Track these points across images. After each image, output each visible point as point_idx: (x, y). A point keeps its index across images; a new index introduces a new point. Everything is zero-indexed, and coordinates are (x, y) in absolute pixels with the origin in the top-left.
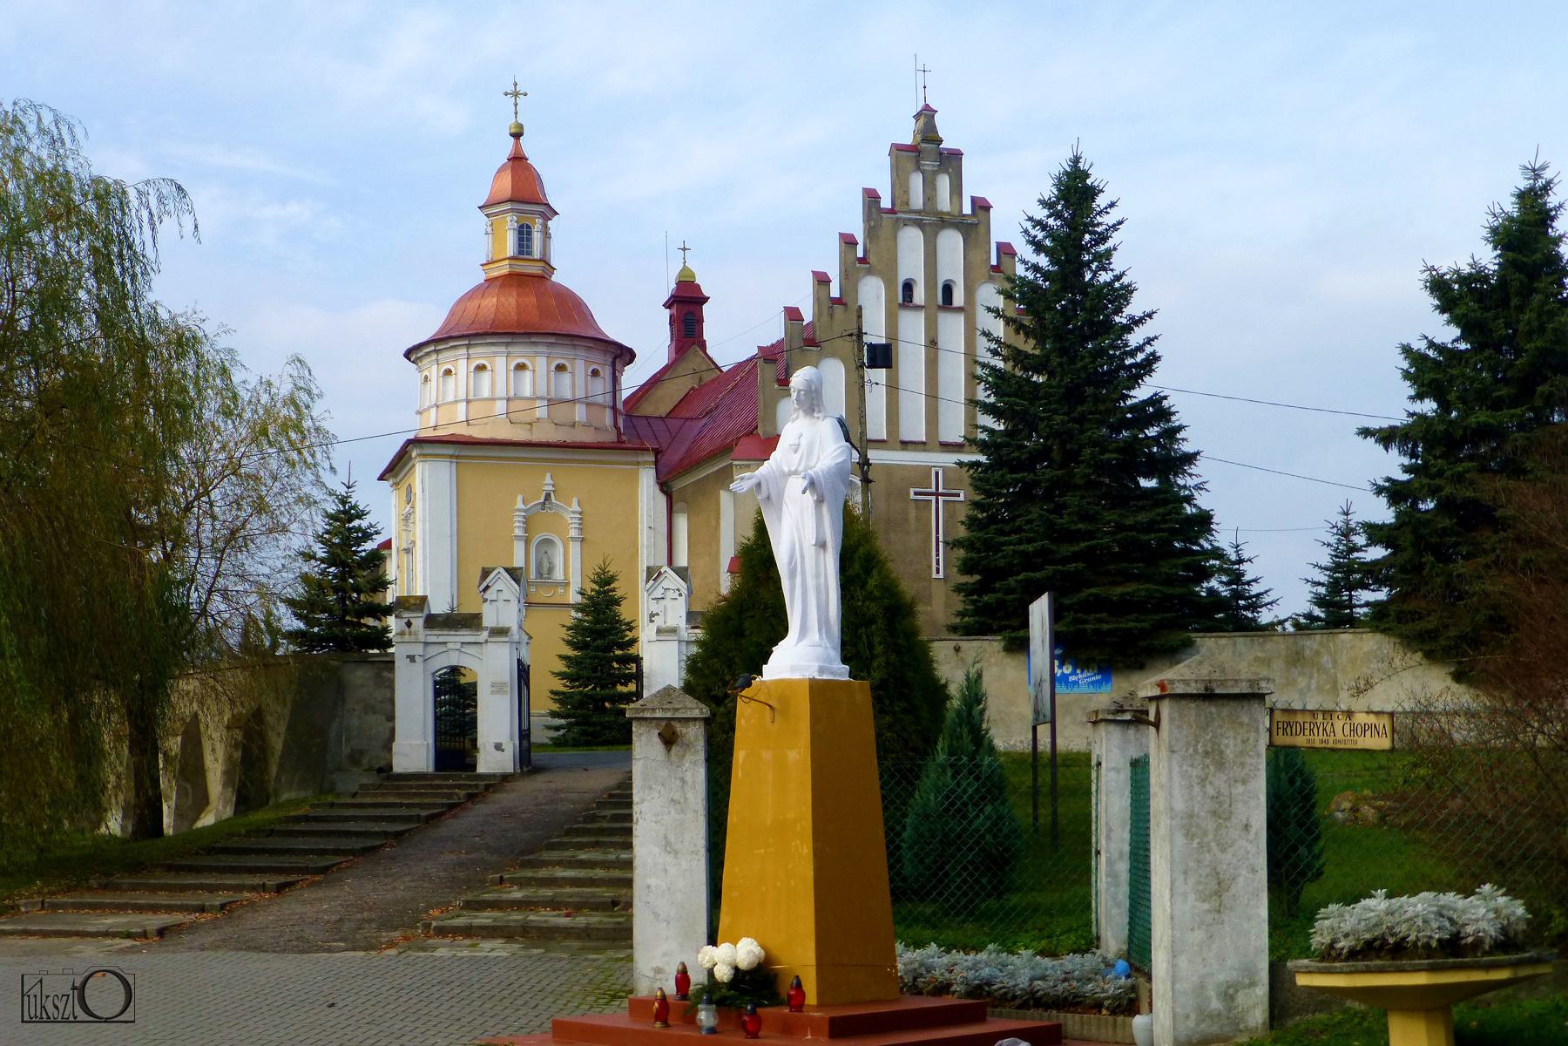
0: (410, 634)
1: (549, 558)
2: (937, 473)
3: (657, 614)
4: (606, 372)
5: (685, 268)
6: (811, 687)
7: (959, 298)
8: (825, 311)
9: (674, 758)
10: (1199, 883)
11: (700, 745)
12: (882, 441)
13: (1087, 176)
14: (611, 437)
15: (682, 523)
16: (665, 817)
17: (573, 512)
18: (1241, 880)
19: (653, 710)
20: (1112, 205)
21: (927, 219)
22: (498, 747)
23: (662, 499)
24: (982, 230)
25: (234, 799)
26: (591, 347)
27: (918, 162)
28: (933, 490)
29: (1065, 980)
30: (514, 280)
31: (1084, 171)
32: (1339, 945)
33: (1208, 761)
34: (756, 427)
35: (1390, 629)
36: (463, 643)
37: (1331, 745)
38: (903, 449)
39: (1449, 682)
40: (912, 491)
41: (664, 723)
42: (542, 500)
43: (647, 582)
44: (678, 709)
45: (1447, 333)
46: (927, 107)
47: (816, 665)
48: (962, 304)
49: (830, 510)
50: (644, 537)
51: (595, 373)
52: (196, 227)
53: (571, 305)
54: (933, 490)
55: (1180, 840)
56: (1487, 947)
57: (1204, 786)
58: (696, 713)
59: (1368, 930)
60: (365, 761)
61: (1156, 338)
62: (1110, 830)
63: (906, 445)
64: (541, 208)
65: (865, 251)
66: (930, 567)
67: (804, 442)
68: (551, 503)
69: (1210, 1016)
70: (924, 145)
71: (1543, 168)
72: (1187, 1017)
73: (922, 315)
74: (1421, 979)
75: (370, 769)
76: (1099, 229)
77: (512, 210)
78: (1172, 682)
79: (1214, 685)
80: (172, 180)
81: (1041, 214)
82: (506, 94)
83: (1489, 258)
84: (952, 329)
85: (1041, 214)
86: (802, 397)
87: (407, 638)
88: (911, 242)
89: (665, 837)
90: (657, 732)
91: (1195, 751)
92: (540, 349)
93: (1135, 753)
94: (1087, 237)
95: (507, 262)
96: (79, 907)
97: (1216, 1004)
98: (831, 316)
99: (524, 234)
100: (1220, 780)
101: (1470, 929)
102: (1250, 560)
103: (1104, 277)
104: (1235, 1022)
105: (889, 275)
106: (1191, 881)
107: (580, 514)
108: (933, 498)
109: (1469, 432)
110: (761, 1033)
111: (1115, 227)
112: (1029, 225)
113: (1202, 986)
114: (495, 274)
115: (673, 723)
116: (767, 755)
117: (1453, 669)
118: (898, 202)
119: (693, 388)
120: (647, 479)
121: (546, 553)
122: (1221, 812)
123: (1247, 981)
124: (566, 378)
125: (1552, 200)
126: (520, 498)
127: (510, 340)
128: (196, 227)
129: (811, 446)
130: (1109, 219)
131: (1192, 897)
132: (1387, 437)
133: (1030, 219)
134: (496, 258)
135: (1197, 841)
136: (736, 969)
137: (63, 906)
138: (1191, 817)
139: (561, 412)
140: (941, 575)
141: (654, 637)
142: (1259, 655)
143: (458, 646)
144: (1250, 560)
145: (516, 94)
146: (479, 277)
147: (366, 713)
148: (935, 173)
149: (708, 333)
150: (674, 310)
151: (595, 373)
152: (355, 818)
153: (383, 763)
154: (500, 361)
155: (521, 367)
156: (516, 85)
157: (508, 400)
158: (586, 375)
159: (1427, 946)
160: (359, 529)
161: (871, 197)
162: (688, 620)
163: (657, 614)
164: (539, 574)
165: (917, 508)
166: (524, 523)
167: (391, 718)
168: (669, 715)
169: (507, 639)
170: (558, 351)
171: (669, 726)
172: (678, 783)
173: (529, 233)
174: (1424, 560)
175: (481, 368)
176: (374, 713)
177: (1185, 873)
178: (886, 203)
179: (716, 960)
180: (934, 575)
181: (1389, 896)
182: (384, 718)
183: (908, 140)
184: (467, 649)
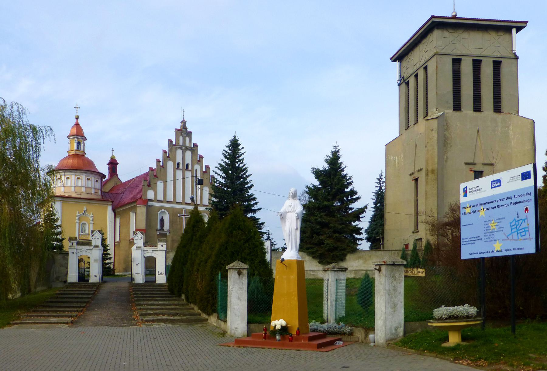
0: (73, 246)
1: (84, 228)
2: (184, 210)
3: (136, 243)
4: (99, 181)
5: (113, 155)
6: (297, 262)
7: (190, 168)
8: (159, 169)
9: (240, 278)
10: (391, 305)
11: (247, 275)
12: (172, 202)
13: (238, 141)
14: (100, 197)
15: (118, 220)
16: (238, 292)
17: (91, 216)
18: (399, 305)
19: (236, 266)
20: (242, 148)
21: (183, 148)
22: (95, 276)
23: (113, 214)
24: (196, 151)
26: (86, 173)
27: (182, 133)
28: (183, 214)
29: (335, 328)
30: (76, 156)
31: (237, 139)
32: (443, 317)
33: (393, 279)
34: (142, 197)
35: (305, 251)
36: (86, 249)
37: (414, 275)
38: (168, 203)
39: (318, 264)
40: (178, 214)
41: (238, 270)
42: (83, 213)
43: (134, 235)
44: (242, 266)
45: (317, 183)
46: (184, 120)
47: (296, 256)
48: (191, 169)
49: (300, 221)
50: (108, 223)
51: (97, 181)
52: (55, 139)
53: (90, 163)
54: (183, 214)
55: (387, 296)
56: (474, 317)
57: (392, 284)
58: (246, 267)
59: (450, 313)
60: (60, 279)
61: (252, 180)
62: (331, 295)
63: (177, 203)
64: (83, 138)
65: (169, 155)
67: (293, 205)
68: (85, 214)
69: (393, 334)
70: (183, 130)
71: (338, 146)
72: (388, 334)
73: (182, 171)
74: (464, 323)
75: (61, 281)
76: (240, 154)
77: (76, 138)
78: (387, 261)
79: (395, 262)
80: (49, 127)
81: (227, 149)
82: (75, 107)
83: (326, 166)
84: (188, 174)
85: (227, 149)
86: (293, 195)
87: (72, 247)
88: (179, 153)
89: (238, 296)
90: (237, 272)
91: (390, 276)
92: (83, 174)
93: (336, 277)
94: (237, 156)
95: (74, 151)
96: (37, 316)
97: (394, 332)
98: (161, 170)
99: (79, 144)
100: (395, 283)
101: (471, 313)
102: (271, 234)
103: (241, 166)
104: (397, 335)
106: (389, 305)
107: (93, 217)
109: (323, 206)
110: (293, 341)
111: (243, 153)
112: (224, 152)
113: (391, 328)
114: (71, 154)
115: (240, 269)
116: (285, 277)
117: (318, 260)
118: (177, 143)
119: (114, 186)
120: (109, 208)
121: (84, 226)
122: (395, 290)
123: (399, 326)
124: (90, 182)
125: (340, 154)
126: (78, 212)
127: (96, 174)
128: (55, 139)
129: (294, 206)
130: (242, 151)
131: (389, 308)
132: (373, 208)
133: (224, 150)
134: (71, 150)
135: (390, 296)
136: (282, 326)
137: (33, 316)
138: (389, 291)
139: (88, 191)
141: (135, 249)
142: (276, 256)
143: (152, 251)
144: (271, 234)
145: (77, 108)
146: (66, 155)
147: (60, 267)
148: (186, 137)
150: (110, 166)
151: (97, 181)
152: (75, 294)
153: (65, 280)
154: (73, 177)
155: (78, 178)
156: (77, 105)
157: (75, 187)
159: (463, 317)
160: (54, 219)
161: (170, 141)
162: (144, 245)
163: (136, 243)
164: (82, 232)
165: (179, 218)
166: (79, 219)
167: (67, 268)
168: (240, 268)
169: (98, 249)
170: (88, 175)
171: (239, 270)
172: (241, 284)
173: (80, 144)
174: (314, 235)
176: (63, 267)
177: (388, 303)
178: (174, 143)
179: (276, 324)
181: (445, 307)
182: (65, 268)
183: (179, 128)
184: (89, 251)
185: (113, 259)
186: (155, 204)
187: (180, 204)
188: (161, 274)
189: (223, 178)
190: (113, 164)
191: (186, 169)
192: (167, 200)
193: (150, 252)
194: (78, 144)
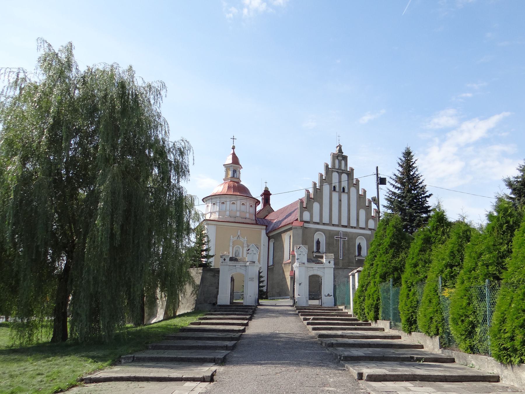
5: (266, 188)
7: (346, 190)
25: (164, 313)
28: (340, 237)
40: (335, 237)
51: (251, 206)
54: (340, 237)
63: (333, 225)
66: (339, 256)
84: (344, 197)
87: (224, 264)
88: (335, 175)
105: (330, 184)
108: (340, 239)
120: (264, 232)
140: (342, 258)
143: (239, 267)
145: (234, 139)
149: (271, 202)
151: (251, 206)
153: (214, 302)
158: (249, 206)
161: (327, 166)
167: (218, 288)
173: (236, 172)
175: (223, 203)
180: (340, 258)
185: (266, 287)
186: (311, 226)
187: (336, 226)
188: (328, 295)
189: (399, 188)
190: (267, 195)
191: (342, 191)
192: (324, 222)
193: (315, 269)
194: (234, 171)
